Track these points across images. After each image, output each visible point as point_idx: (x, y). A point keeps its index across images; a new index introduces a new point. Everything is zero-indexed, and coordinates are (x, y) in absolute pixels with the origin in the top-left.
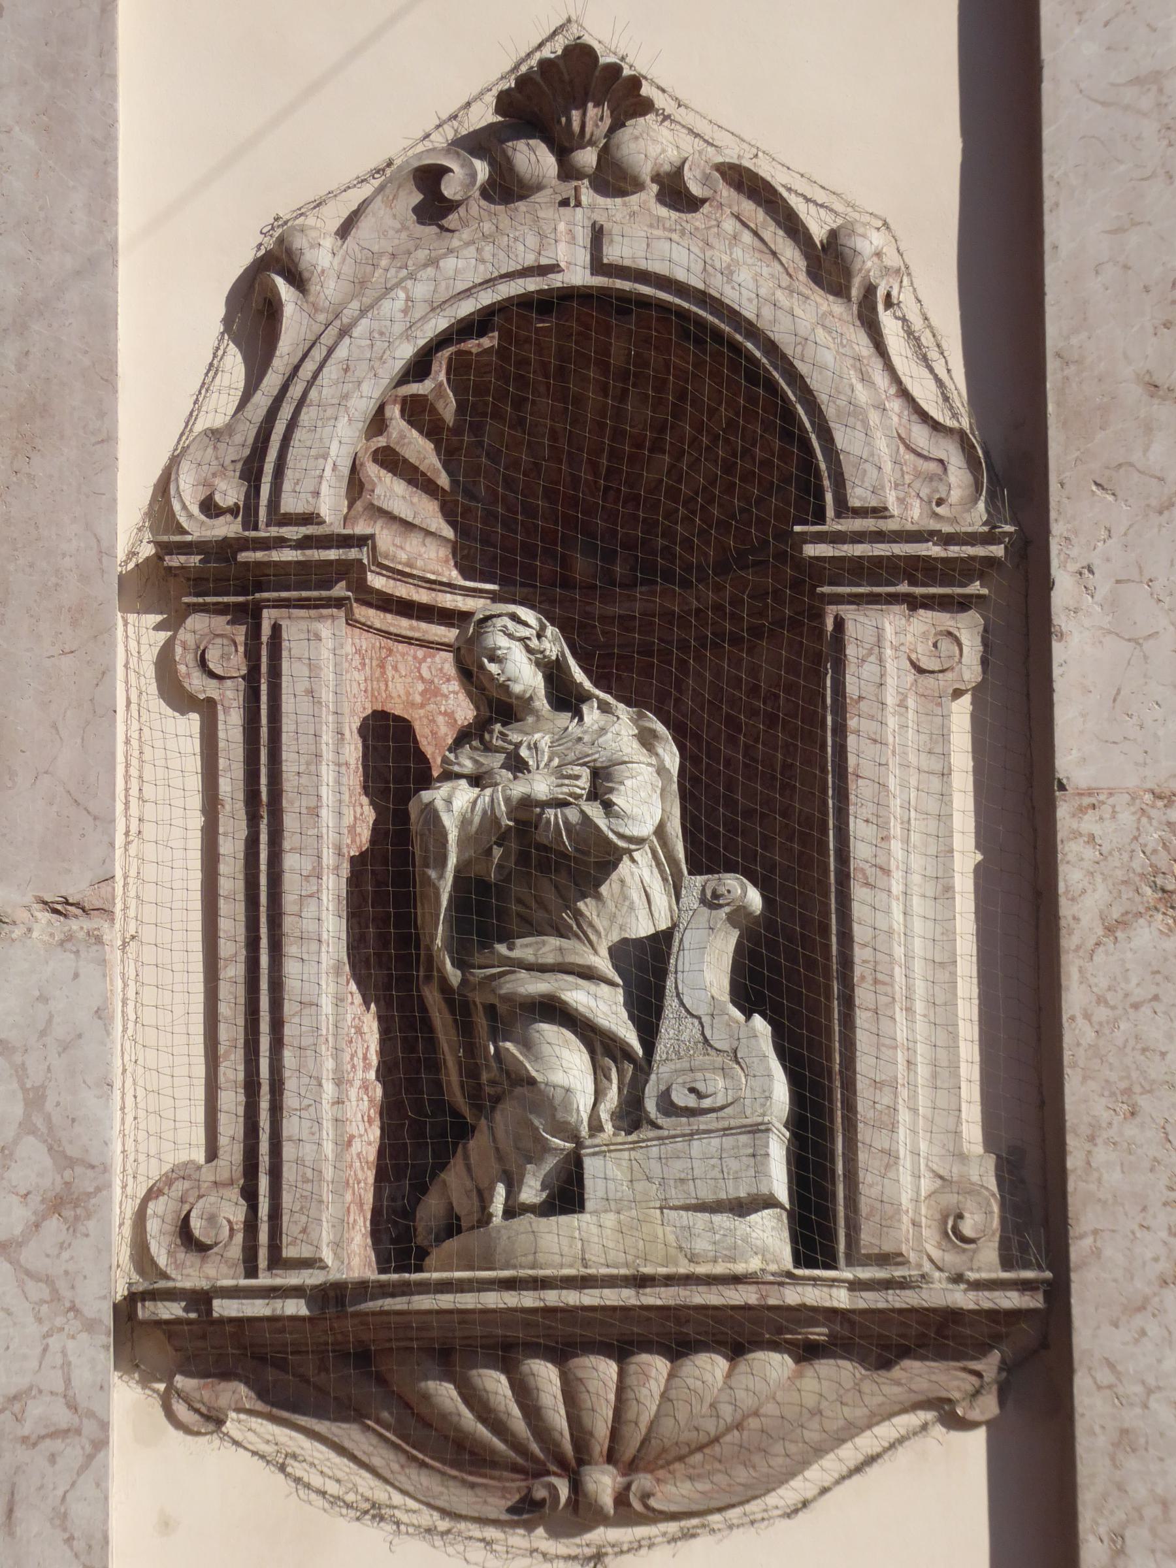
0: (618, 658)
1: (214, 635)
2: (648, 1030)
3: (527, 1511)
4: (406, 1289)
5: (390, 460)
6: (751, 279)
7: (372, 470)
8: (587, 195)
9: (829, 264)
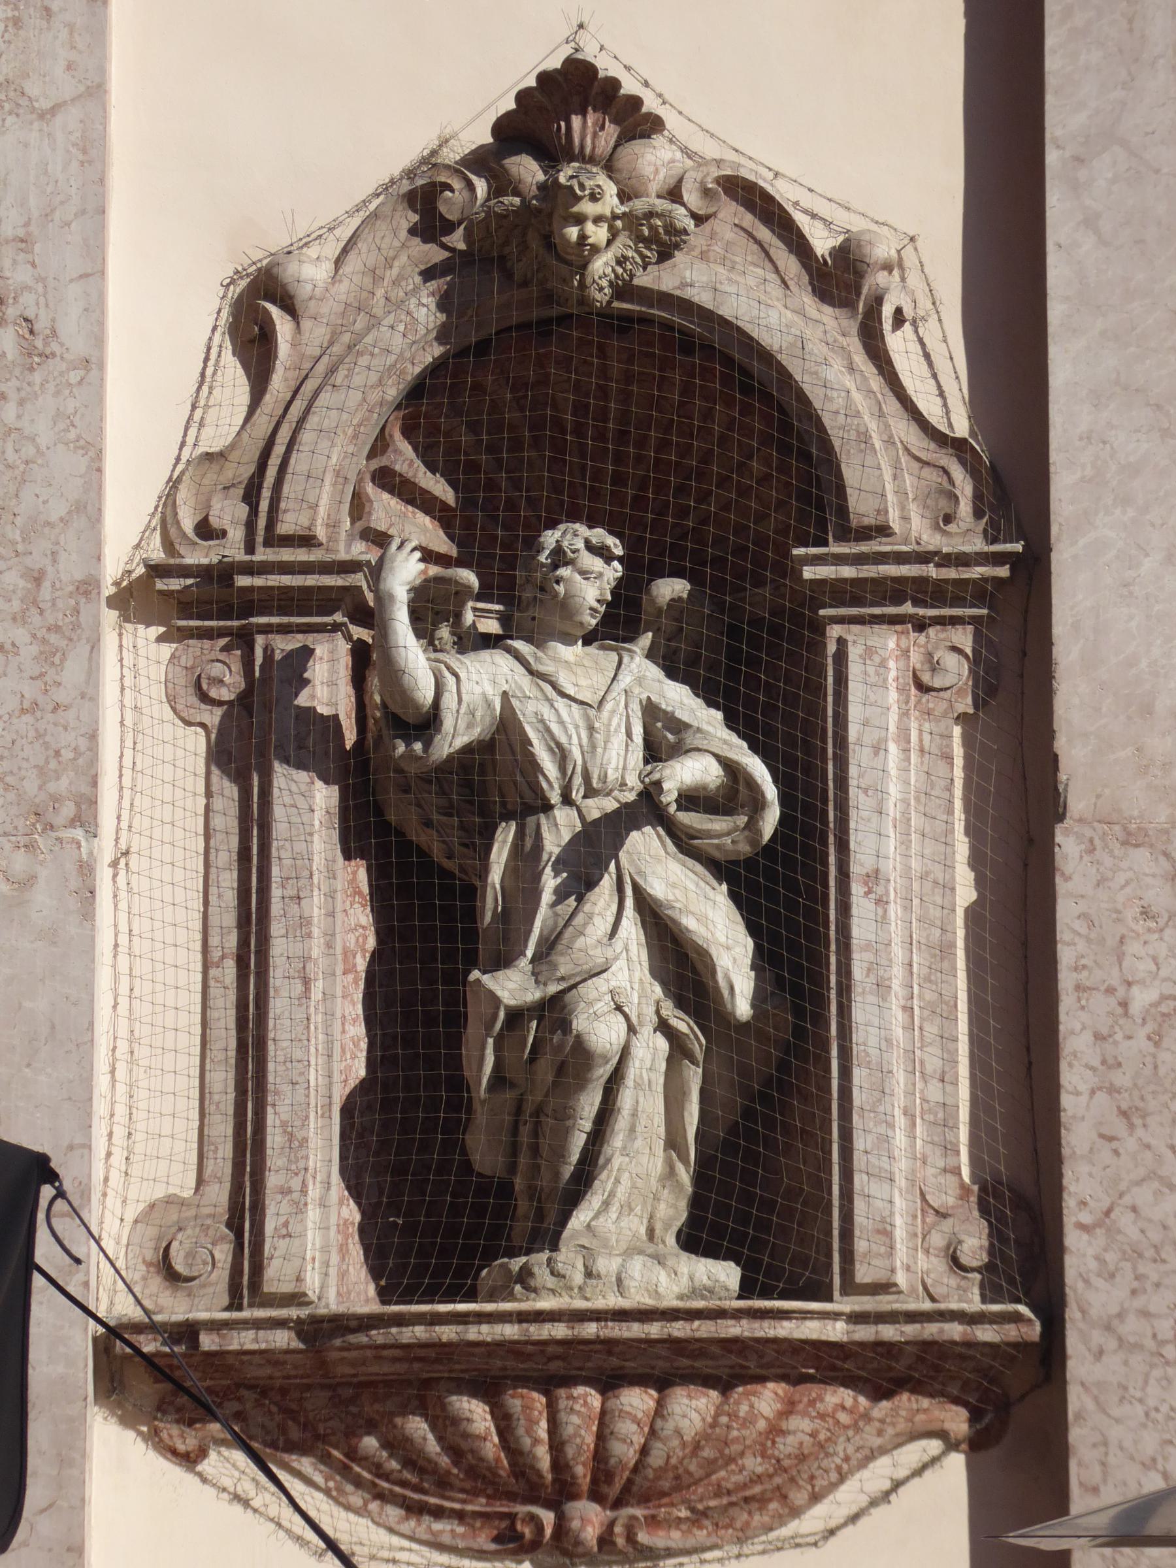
4: (400, 1320)
5: (387, 479)
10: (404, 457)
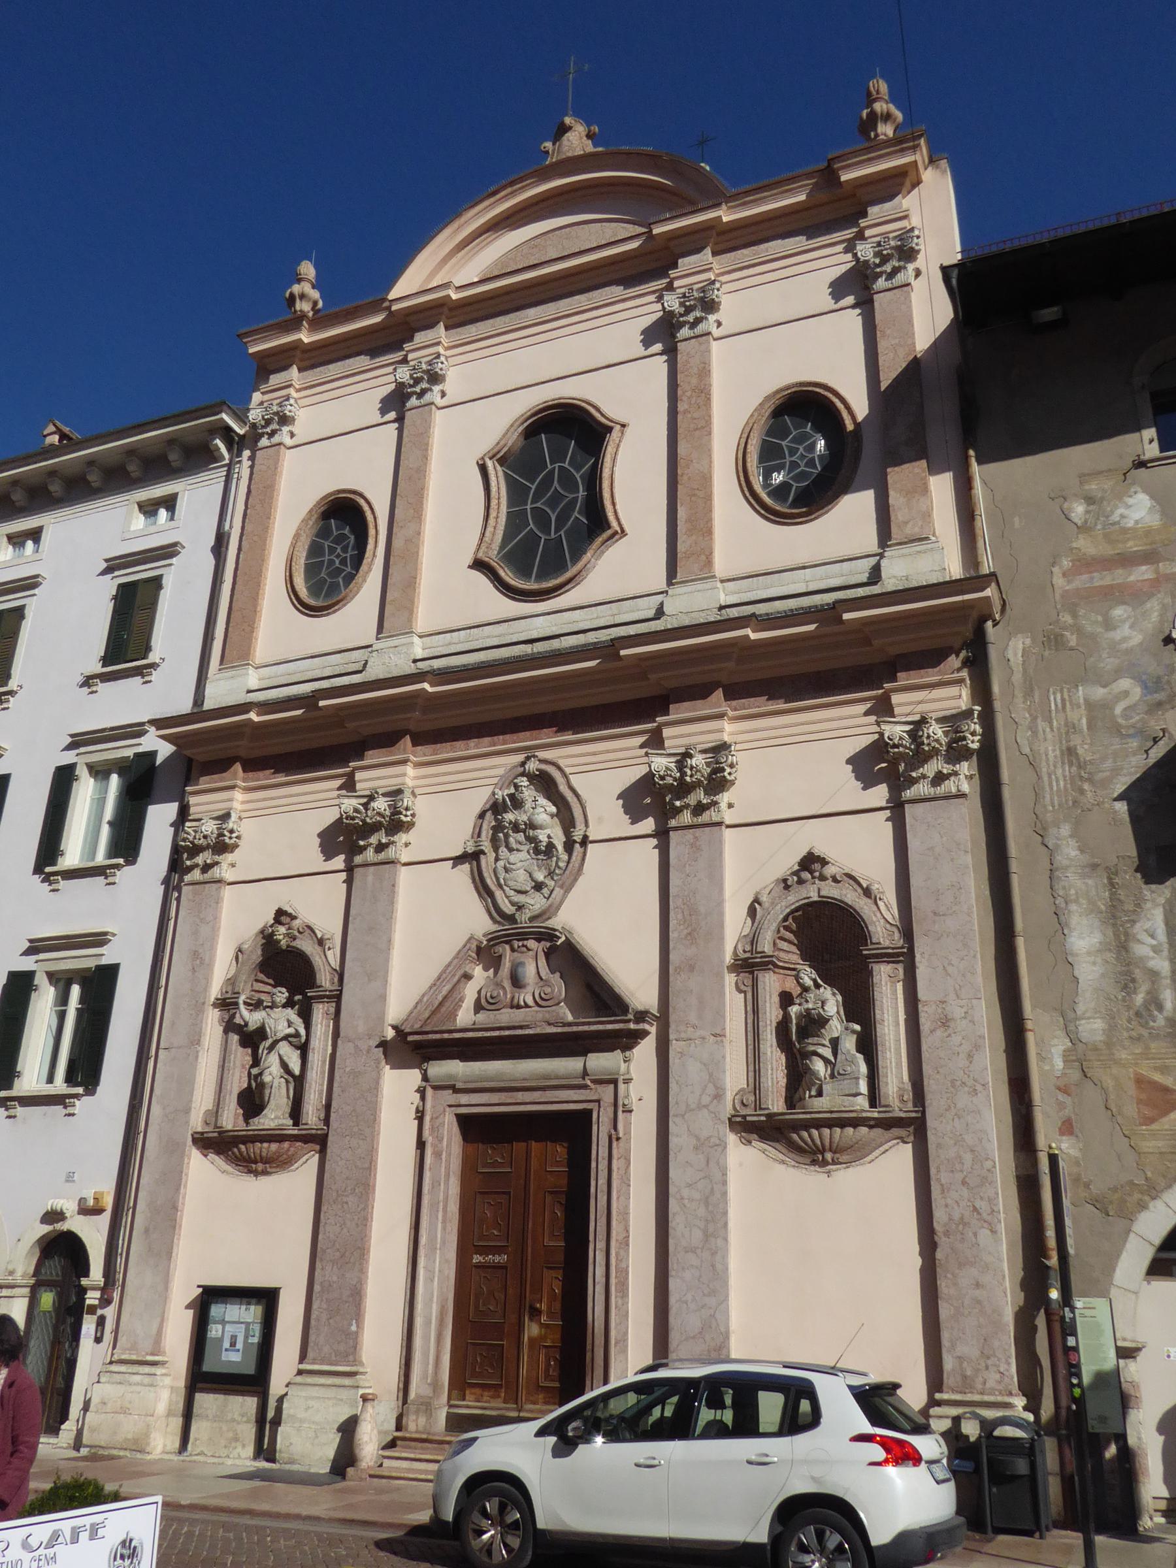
0: (828, 977)
1: (746, 978)
2: (836, 1058)
3: (814, 1162)
5: (781, 938)
6: (850, 896)
7: (778, 941)
8: (817, 881)
9: (867, 892)
10: (261, 976)
